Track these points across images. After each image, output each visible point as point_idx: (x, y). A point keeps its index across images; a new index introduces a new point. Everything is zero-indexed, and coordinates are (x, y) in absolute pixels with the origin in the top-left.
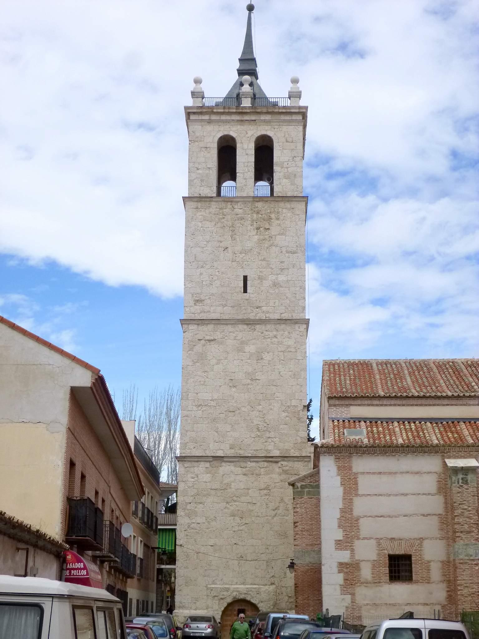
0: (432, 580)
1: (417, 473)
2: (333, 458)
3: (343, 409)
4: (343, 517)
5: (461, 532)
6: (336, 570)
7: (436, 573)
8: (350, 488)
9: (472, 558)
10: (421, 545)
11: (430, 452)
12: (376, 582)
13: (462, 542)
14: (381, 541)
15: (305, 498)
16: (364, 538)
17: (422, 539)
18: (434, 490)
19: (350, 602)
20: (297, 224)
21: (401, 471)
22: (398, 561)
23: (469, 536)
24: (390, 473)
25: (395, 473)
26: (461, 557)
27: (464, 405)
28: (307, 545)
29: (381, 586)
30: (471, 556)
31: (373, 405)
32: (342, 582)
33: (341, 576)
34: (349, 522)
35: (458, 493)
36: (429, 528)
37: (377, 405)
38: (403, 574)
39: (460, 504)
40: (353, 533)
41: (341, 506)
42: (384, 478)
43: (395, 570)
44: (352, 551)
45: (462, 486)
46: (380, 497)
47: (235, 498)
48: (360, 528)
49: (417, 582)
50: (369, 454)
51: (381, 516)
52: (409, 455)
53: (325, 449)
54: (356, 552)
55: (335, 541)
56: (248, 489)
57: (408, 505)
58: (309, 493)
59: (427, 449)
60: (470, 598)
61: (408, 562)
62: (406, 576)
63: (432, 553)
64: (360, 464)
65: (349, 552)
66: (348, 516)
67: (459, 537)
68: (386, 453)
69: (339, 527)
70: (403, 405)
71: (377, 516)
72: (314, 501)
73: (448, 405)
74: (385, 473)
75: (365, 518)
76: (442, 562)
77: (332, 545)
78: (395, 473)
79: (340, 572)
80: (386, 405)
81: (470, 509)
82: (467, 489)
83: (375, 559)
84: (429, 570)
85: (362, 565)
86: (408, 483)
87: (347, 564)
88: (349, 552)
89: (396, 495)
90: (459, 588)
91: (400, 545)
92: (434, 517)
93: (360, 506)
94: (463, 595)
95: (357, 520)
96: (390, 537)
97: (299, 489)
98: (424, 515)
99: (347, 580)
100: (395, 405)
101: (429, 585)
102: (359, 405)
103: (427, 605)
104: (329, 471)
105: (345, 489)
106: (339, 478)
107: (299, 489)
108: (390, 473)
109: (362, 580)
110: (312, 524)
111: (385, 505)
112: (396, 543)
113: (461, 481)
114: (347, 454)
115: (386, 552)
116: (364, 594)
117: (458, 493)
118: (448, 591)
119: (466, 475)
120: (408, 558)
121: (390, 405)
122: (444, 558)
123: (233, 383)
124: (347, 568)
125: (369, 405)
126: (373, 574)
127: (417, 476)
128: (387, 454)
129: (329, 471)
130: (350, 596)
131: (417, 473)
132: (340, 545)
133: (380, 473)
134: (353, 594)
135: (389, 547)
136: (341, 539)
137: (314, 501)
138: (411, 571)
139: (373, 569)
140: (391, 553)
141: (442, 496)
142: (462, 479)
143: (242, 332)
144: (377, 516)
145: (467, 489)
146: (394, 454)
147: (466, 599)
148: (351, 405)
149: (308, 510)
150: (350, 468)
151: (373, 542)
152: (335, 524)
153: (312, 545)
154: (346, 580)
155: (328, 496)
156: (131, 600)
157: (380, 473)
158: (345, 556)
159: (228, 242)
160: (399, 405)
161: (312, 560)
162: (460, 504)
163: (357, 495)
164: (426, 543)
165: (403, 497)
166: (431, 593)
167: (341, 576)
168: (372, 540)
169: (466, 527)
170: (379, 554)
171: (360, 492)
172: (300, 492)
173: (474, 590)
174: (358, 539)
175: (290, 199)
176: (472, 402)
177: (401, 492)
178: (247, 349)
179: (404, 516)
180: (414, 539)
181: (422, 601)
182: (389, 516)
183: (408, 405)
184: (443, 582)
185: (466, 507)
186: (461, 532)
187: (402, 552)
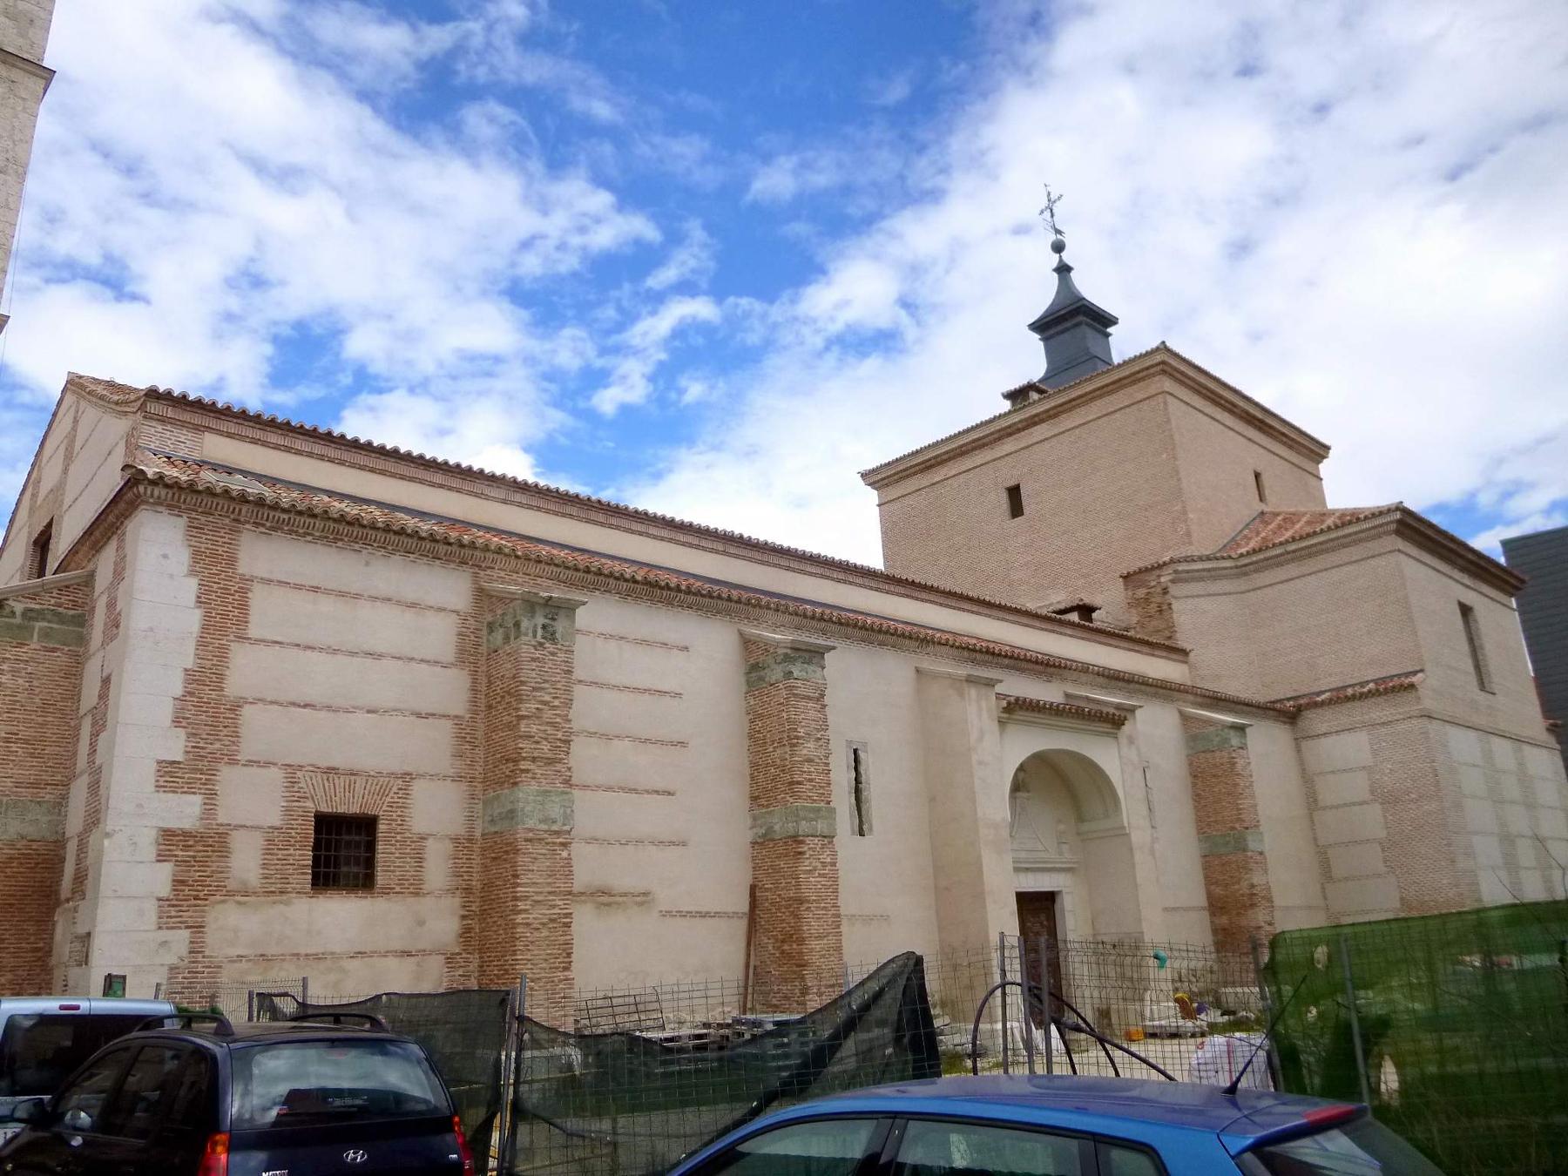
0: (426, 887)
1: (413, 605)
2: (182, 522)
3: (185, 435)
4: (191, 694)
5: (534, 760)
6: (150, 852)
7: (437, 869)
8: (224, 616)
9: (555, 828)
10: (405, 792)
11: (447, 559)
12: (275, 891)
13: (534, 786)
14: (299, 774)
15: (33, 646)
16: (250, 763)
17: (407, 777)
18: (448, 652)
19: (184, 951)
20: (16, 116)
21: (374, 593)
22: (339, 833)
23: (550, 770)
24: (342, 594)
25: (357, 596)
26: (530, 823)
27: (476, 495)
28: (18, 785)
29: (287, 903)
30: (554, 822)
31: (265, 444)
32: (165, 890)
33: (167, 869)
34: (209, 712)
35: (534, 660)
36: (429, 748)
37: (277, 447)
38: (344, 869)
39: (535, 689)
40: (217, 745)
41: (190, 662)
42: (326, 605)
43: (327, 858)
44: (211, 795)
45: (541, 644)
46: (309, 652)
48: (243, 731)
49: (387, 891)
50: (290, 532)
51: (305, 706)
52: (396, 558)
53: (164, 492)
54: (220, 800)
55: (159, 762)
57: (382, 684)
58: (46, 635)
59: (442, 548)
60: (545, 933)
61: (364, 838)
62: (356, 876)
63: (433, 815)
64: (260, 555)
65: (197, 800)
66: (208, 693)
67: (527, 771)
68: (336, 540)
69: (177, 722)
70: (342, 463)
71: (294, 704)
72: (61, 659)
73: (441, 486)
74: (328, 592)
75: (261, 705)
76: (455, 840)
77: (147, 773)
78: (357, 596)
79: (161, 858)
80: (299, 453)
81: (556, 703)
82: (553, 654)
83: (278, 823)
84: (420, 860)
85: (238, 841)
86: (385, 628)
87: (186, 834)
88: (197, 800)
89: (353, 654)
90: (521, 905)
91: (350, 787)
92: (443, 721)
93: (246, 670)
94: (528, 924)
95: (236, 707)
96: (324, 764)
97: (18, 620)
98: (419, 715)
99: (182, 882)
100: (321, 457)
101: (421, 899)
102: (229, 435)
103: (409, 954)
104: (165, 556)
105: (207, 615)
106: (192, 584)
107: (18, 620)
108: (342, 594)
109: (232, 885)
110: (42, 725)
111: (321, 676)
112: (341, 782)
113: (540, 632)
114: (227, 521)
115: (309, 804)
116: (237, 929)
117: (534, 660)
118: (464, 917)
119: (553, 619)
120: (365, 826)
121: (310, 455)
122: (460, 830)
124: (187, 847)
125: (254, 441)
126: (265, 866)
127: (409, 615)
128: (340, 544)
129: (165, 556)
130: (185, 934)
131: (413, 605)
132: (170, 776)
133: (315, 589)
134: (198, 928)
135: (320, 792)
136: (179, 758)
137: (61, 659)
138: (370, 863)
139: (268, 851)
140: (324, 808)
141: (465, 672)
142: (544, 627)
144: (294, 704)
145: (553, 654)
146: (357, 547)
147: (536, 934)
148: (209, 429)
149: (35, 683)
150: (232, 561)
151: (276, 775)
152: (165, 711)
153: (35, 785)
154: (178, 883)
155: (151, 629)
156: (62, 1008)
157: (315, 589)
158: (185, 811)
160: (331, 461)
161: (30, 831)
162: (535, 689)
163: (242, 638)
164: (419, 788)
165: (369, 661)
166: (421, 923)
167: (167, 869)
168: (274, 769)
169: (545, 746)
170: (288, 811)
171: (253, 631)
172: (19, 627)
173: (556, 911)
174: (233, 762)
175: (10, 59)
176: (494, 492)
177: (366, 648)
179: (369, 712)
180: (390, 774)
181: (398, 946)
182: (329, 708)
183: (353, 466)
184: (452, 891)
185: (547, 698)
186: (534, 760)
187: (354, 809)
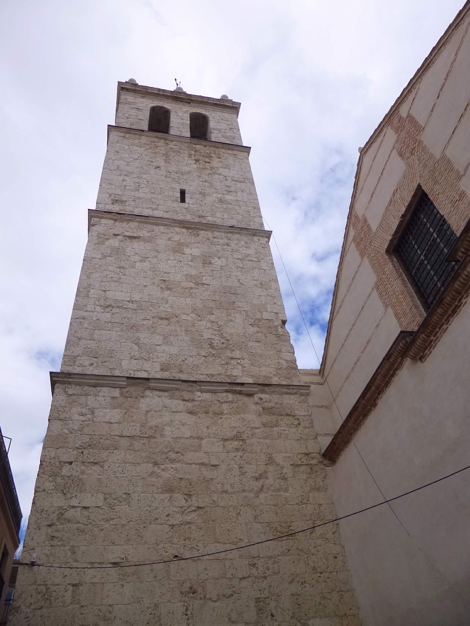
47: (172, 455)
56: (200, 438)
123: (167, 285)
143: (179, 235)
159: (162, 163)
178: (187, 251)
